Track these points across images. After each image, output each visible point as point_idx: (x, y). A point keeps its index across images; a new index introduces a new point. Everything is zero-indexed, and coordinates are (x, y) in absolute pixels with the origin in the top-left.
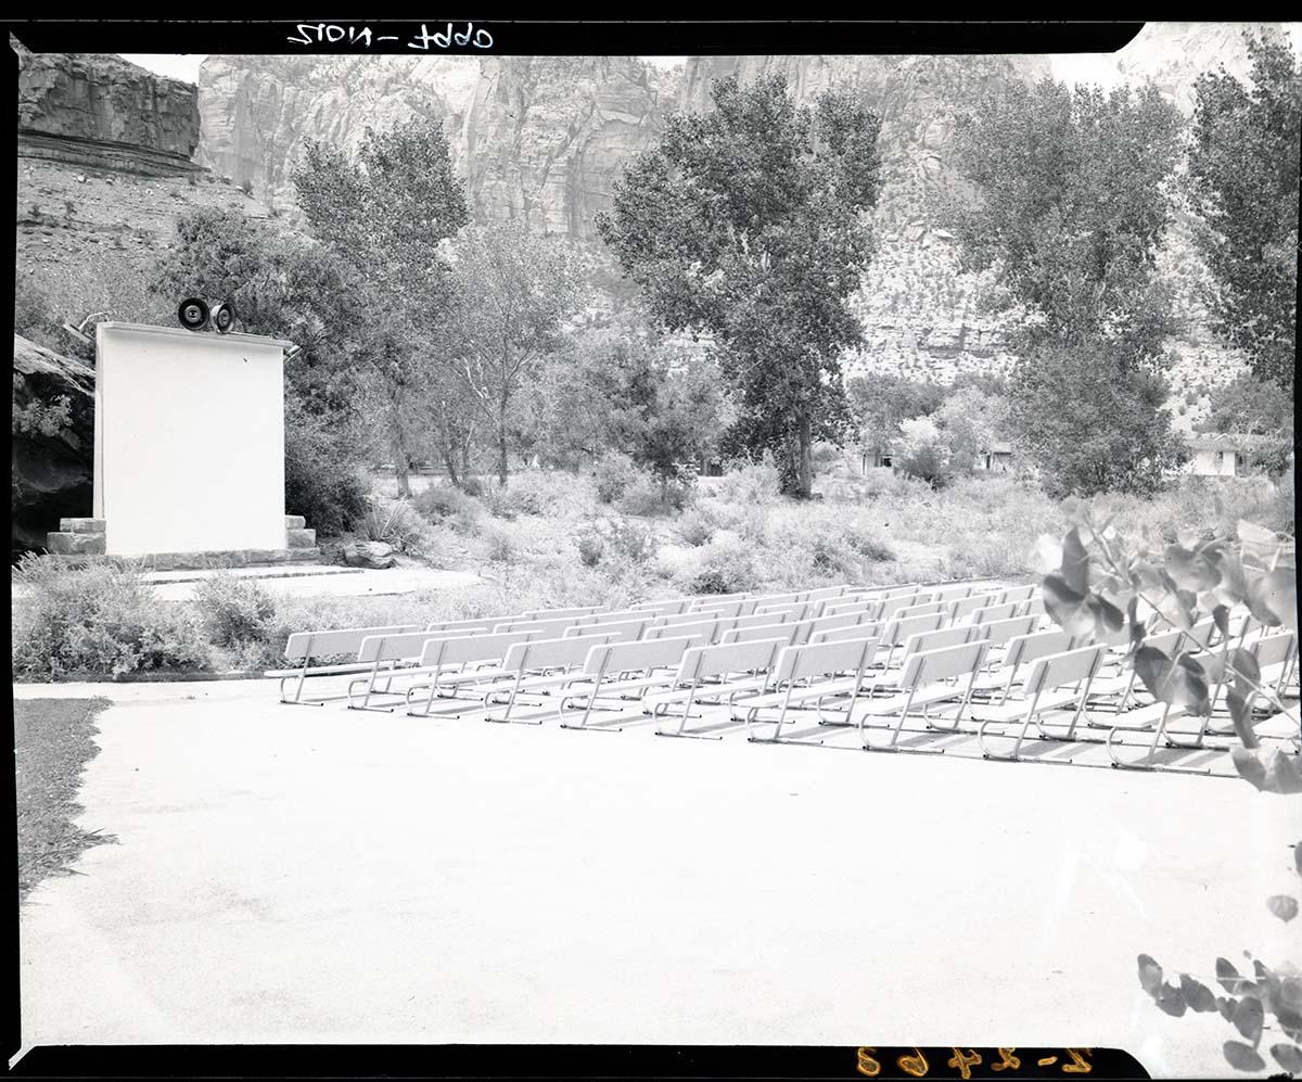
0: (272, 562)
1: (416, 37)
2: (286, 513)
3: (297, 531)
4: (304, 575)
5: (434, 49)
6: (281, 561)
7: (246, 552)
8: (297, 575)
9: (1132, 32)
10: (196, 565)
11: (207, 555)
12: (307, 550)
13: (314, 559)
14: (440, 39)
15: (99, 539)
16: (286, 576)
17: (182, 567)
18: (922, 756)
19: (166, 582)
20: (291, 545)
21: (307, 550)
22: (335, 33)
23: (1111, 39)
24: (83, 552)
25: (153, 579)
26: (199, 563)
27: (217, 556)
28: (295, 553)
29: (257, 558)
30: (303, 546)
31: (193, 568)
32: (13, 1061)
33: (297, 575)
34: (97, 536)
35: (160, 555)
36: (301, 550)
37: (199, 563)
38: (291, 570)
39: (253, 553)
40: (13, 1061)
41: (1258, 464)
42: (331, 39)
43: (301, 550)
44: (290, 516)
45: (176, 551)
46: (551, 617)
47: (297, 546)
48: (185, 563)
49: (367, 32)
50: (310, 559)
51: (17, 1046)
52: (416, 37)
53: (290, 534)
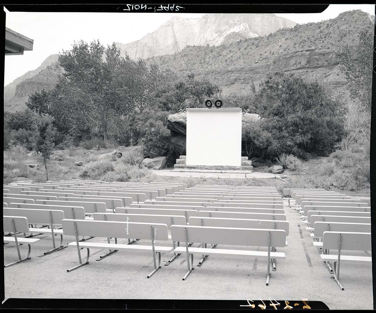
0: (236, 169)
1: (159, 7)
3: (244, 161)
5: (164, 11)
6: (238, 169)
8: (225, 173)
9: (326, 7)
10: (211, 168)
11: (215, 166)
12: (247, 167)
14: (166, 8)
16: (221, 173)
17: (206, 169)
19: (184, 172)
20: (242, 165)
21: (247, 167)
22: (137, 7)
23: (320, 10)
24: (179, 164)
25: (214, 172)
26: (212, 168)
27: (217, 167)
28: (243, 167)
29: (230, 168)
30: (246, 165)
31: (210, 169)
32: (3, 302)
35: (200, 166)
37: (212, 168)
38: (214, 171)
39: (229, 167)
40: (3, 302)
42: (136, 9)
45: (205, 165)
49: (146, 6)
51: (4, 298)
52: (159, 7)
53: (241, 162)
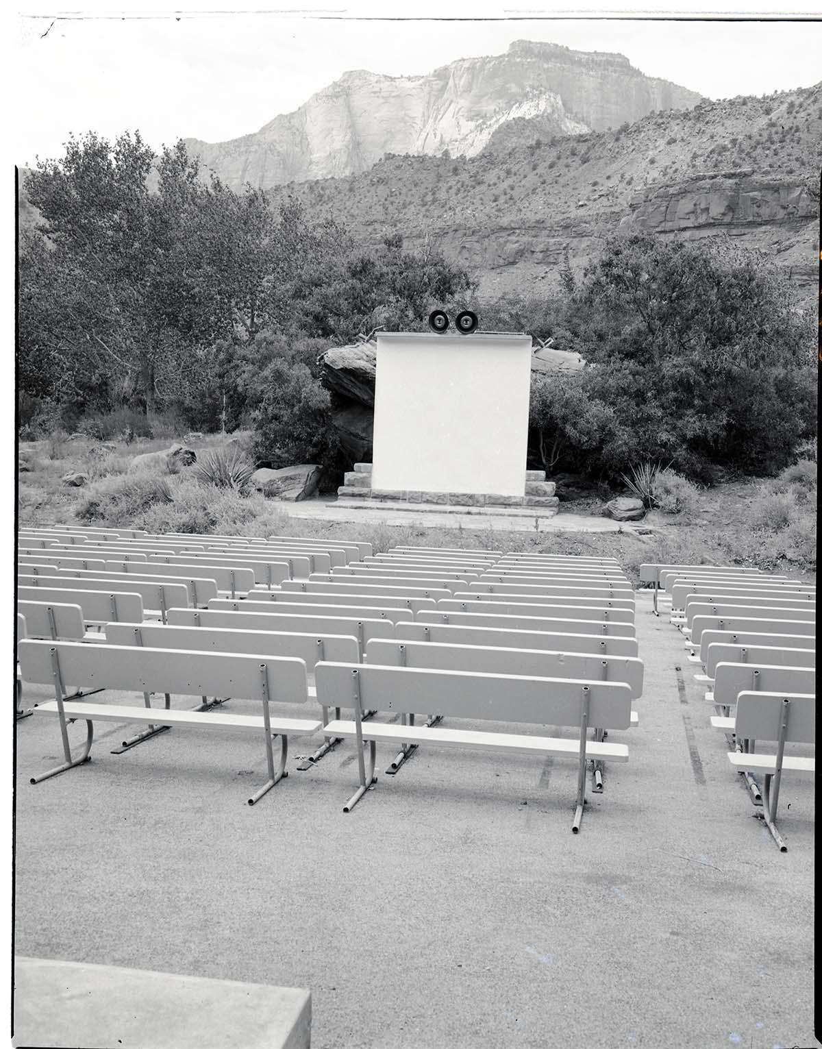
2: (531, 465)
4: (504, 515)
6: (517, 505)
7: (485, 496)
8: (480, 514)
10: (440, 501)
12: (543, 499)
13: (551, 506)
15: (364, 478)
16: (469, 513)
17: (428, 502)
18: (13, 654)
19: (366, 508)
20: (527, 493)
21: (543, 499)
24: (353, 485)
29: (493, 501)
33: (480, 514)
34: (364, 475)
35: (411, 492)
36: (538, 498)
38: (449, 508)
41: (629, 355)
43: (538, 498)
44: (532, 472)
46: (34, 536)
47: (533, 495)
48: (430, 499)
50: (546, 506)
53: (526, 485)
